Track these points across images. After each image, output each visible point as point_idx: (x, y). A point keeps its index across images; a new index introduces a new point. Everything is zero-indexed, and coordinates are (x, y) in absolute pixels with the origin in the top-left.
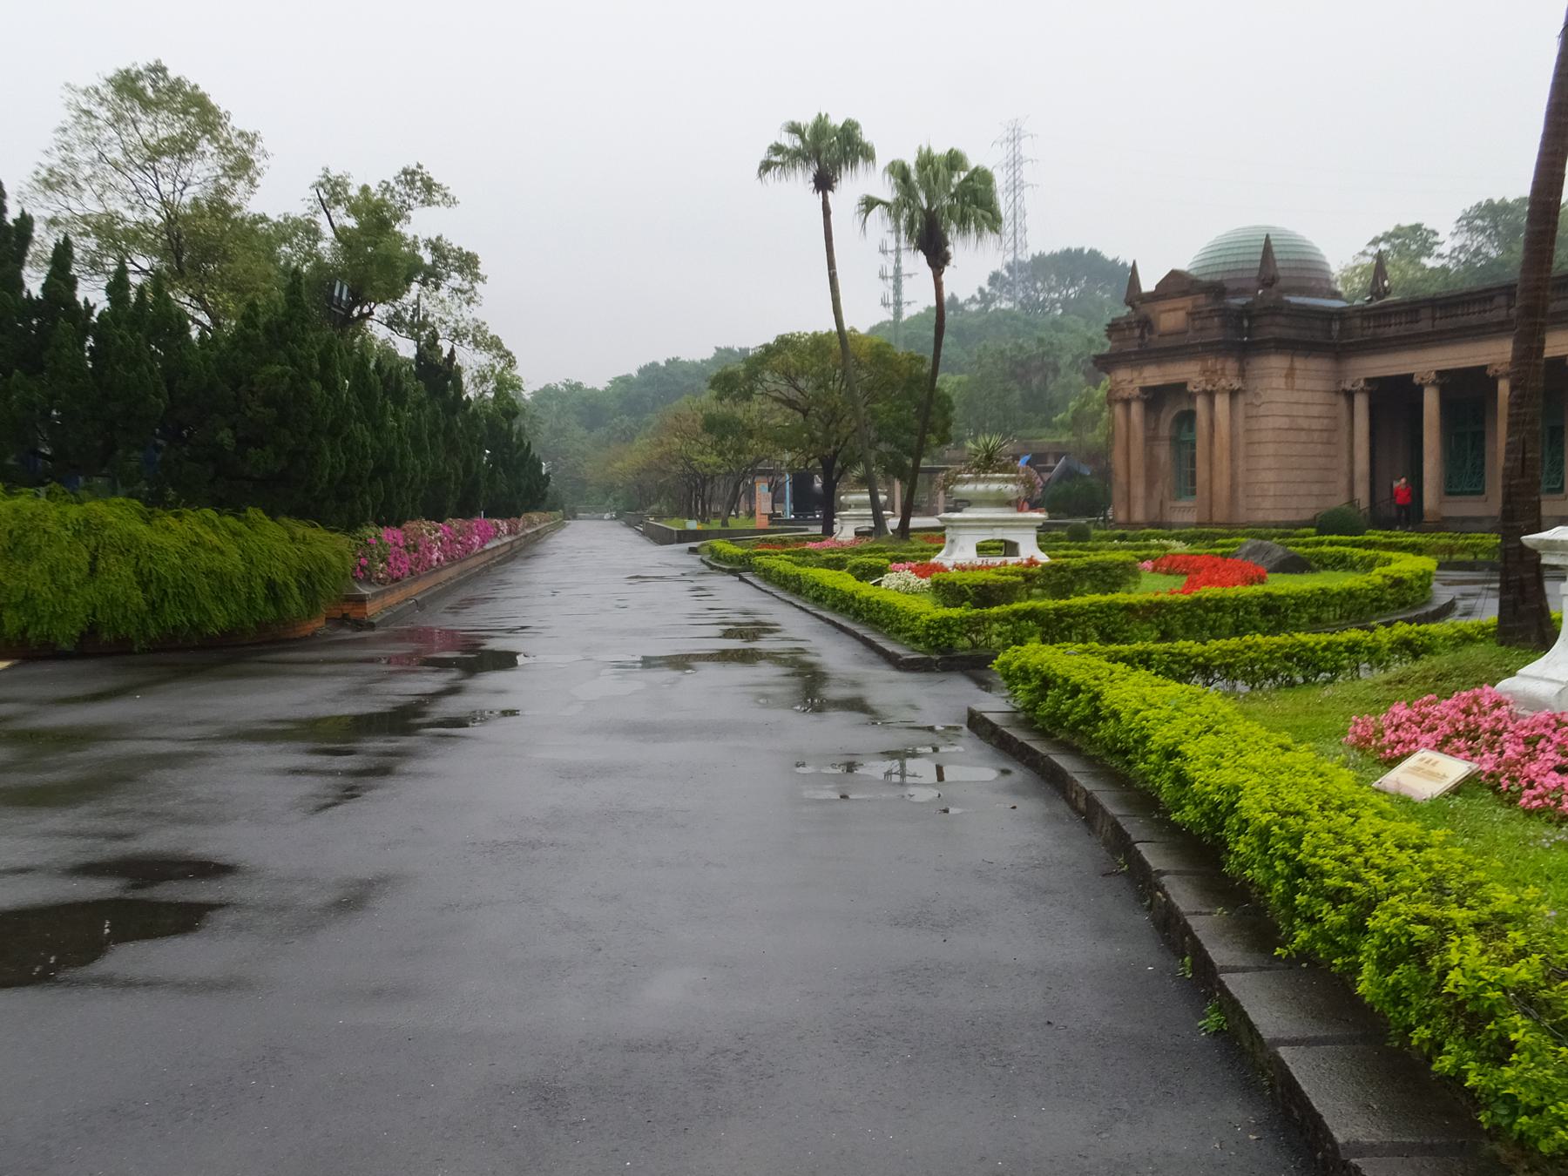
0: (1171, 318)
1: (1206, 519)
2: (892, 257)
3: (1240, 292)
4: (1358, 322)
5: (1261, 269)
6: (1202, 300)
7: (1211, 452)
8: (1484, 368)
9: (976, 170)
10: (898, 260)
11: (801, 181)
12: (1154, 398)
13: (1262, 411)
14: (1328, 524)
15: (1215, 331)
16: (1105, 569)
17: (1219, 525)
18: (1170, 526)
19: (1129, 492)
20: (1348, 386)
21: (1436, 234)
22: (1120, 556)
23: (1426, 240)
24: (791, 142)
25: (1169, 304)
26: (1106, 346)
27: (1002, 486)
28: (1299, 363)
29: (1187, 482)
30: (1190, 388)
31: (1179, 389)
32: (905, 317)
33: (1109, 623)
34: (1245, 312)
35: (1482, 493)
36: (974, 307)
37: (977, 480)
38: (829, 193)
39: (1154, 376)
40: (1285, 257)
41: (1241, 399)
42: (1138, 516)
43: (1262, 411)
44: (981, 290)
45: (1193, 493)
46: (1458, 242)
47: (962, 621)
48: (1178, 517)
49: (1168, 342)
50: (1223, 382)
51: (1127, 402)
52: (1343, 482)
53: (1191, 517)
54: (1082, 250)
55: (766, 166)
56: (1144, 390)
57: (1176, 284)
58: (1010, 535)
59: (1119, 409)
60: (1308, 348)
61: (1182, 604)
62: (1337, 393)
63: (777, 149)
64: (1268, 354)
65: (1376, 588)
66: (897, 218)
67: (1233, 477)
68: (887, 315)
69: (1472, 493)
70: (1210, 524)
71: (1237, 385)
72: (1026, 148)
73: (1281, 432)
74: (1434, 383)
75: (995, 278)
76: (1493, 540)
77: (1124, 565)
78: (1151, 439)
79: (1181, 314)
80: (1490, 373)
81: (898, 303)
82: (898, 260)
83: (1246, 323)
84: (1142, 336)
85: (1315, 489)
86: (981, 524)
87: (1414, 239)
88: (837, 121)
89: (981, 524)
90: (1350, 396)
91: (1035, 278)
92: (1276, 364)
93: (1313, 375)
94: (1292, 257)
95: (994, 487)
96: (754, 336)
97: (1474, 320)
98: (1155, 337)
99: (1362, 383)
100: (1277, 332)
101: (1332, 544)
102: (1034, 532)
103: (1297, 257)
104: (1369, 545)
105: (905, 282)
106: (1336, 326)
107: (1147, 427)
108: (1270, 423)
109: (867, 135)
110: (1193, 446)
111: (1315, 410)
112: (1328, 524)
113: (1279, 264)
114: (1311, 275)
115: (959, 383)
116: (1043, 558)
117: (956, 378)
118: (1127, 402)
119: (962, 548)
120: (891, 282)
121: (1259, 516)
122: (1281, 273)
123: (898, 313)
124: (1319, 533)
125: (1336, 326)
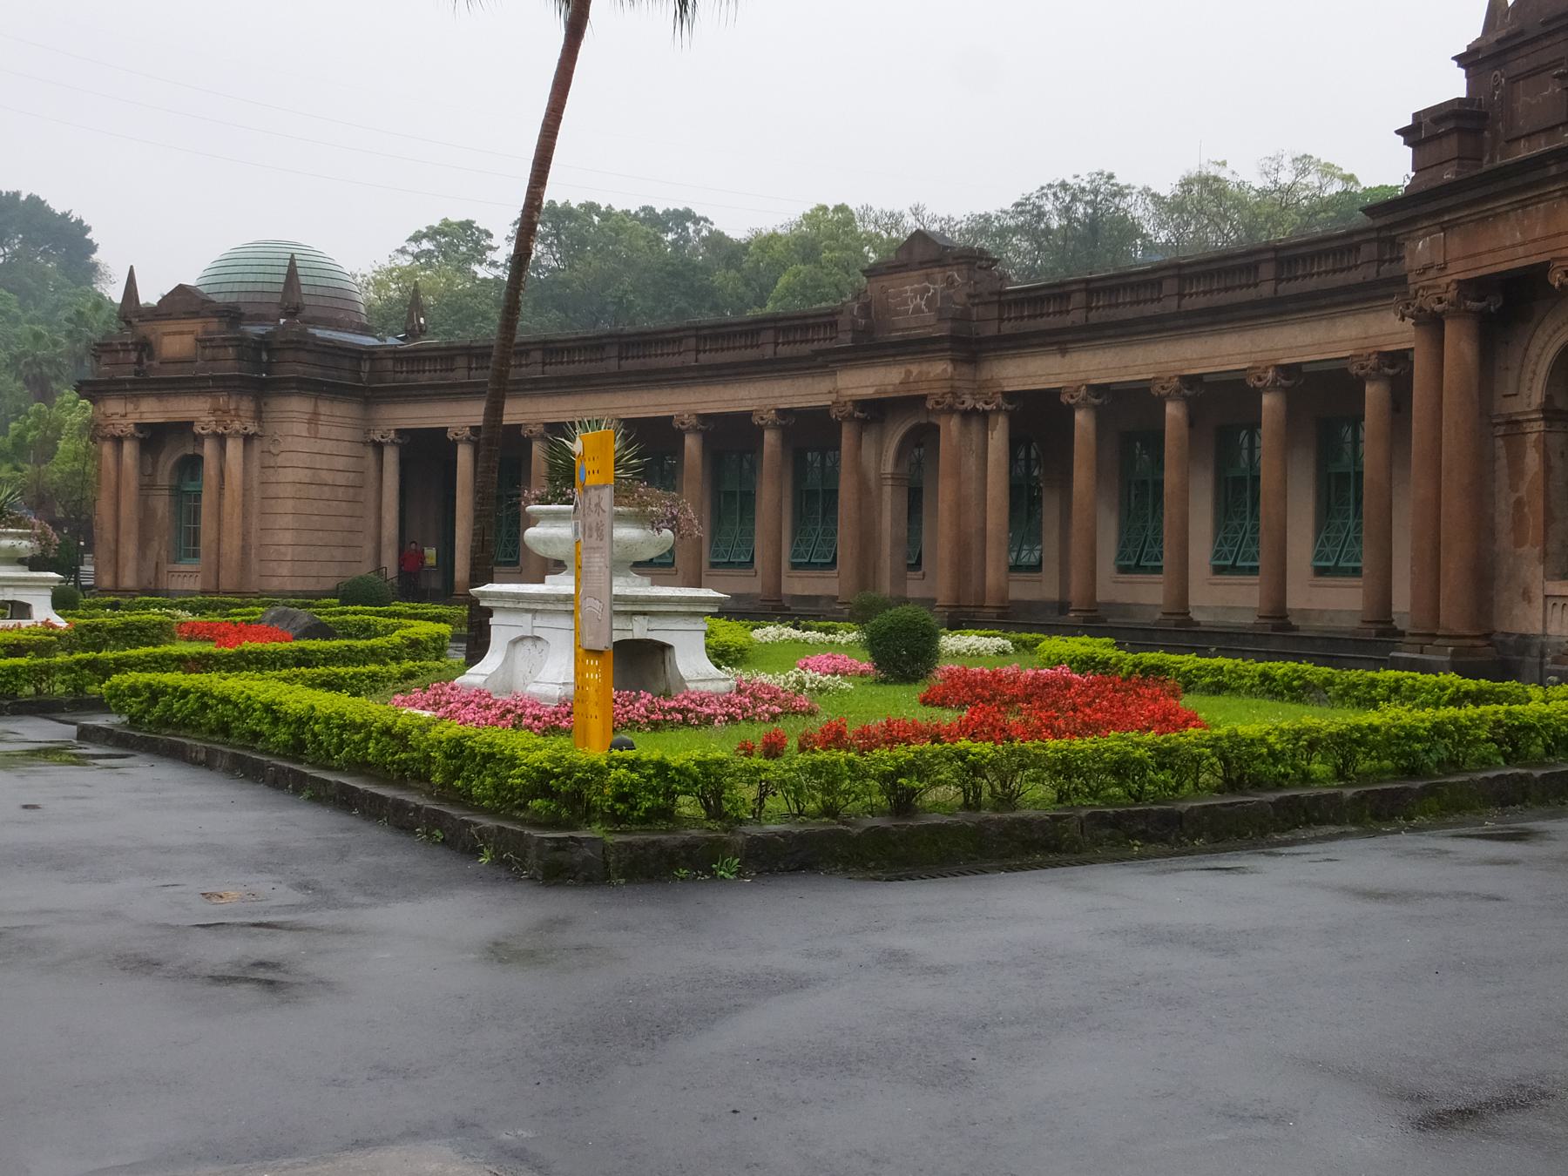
0: (176, 343)
1: (211, 587)
3: (259, 319)
4: (390, 364)
6: (214, 324)
7: (220, 505)
12: (152, 437)
13: (280, 460)
14: (351, 594)
15: (228, 364)
16: (141, 629)
17: (226, 593)
18: (168, 594)
19: (117, 552)
20: (377, 438)
21: (490, 236)
23: (477, 243)
25: (172, 326)
27: (16, 542)
28: (325, 408)
29: (188, 543)
30: (197, 429)
31: (183, 428)
34: (264, 343)
35: (516, 563)
39: (153, 411)
40: (310, 281)
41: (256, 442)
42: (128, 581)
43: (280, 460)
45: (196, 554)
47: (29, 669)
48: (177, 584)
49: (171, 373)
50: (237, 425)
51: (118, 441)
52: (369, 548)
53: (194, 584)
54: (17, 194)
57: (182, 301)
58: (22, 596)
59: (107, 449)
61: (228, 656)
62: (365, 443)
64: (290, 395)
65: (395, 647)
67: (245, 536)
71: (252, 429)
78: (147, 487)
79: (189, 340)
80: (525, 433)
83: (265, 357)
84: (139, 362)
87: (458, 240)
90: (379, 447)
92: (296, 407)
93: (338, 417)
98: (155, 363)
99: (392, 435)
100: (300, 370)
101: (355, 613)
104: (399, 615)
106: (366, 366)
107: (142, 473)
108: (289, 475)
110: (198, 496)
111: (340, 463)
112: (351, 594)
113: (304, 290)
114: (336, 305)
116: (61, 623)
118: (118, 441)
121: (275, 584)
122: (306, 300)
124: (342, 604)
125: (366, 366)
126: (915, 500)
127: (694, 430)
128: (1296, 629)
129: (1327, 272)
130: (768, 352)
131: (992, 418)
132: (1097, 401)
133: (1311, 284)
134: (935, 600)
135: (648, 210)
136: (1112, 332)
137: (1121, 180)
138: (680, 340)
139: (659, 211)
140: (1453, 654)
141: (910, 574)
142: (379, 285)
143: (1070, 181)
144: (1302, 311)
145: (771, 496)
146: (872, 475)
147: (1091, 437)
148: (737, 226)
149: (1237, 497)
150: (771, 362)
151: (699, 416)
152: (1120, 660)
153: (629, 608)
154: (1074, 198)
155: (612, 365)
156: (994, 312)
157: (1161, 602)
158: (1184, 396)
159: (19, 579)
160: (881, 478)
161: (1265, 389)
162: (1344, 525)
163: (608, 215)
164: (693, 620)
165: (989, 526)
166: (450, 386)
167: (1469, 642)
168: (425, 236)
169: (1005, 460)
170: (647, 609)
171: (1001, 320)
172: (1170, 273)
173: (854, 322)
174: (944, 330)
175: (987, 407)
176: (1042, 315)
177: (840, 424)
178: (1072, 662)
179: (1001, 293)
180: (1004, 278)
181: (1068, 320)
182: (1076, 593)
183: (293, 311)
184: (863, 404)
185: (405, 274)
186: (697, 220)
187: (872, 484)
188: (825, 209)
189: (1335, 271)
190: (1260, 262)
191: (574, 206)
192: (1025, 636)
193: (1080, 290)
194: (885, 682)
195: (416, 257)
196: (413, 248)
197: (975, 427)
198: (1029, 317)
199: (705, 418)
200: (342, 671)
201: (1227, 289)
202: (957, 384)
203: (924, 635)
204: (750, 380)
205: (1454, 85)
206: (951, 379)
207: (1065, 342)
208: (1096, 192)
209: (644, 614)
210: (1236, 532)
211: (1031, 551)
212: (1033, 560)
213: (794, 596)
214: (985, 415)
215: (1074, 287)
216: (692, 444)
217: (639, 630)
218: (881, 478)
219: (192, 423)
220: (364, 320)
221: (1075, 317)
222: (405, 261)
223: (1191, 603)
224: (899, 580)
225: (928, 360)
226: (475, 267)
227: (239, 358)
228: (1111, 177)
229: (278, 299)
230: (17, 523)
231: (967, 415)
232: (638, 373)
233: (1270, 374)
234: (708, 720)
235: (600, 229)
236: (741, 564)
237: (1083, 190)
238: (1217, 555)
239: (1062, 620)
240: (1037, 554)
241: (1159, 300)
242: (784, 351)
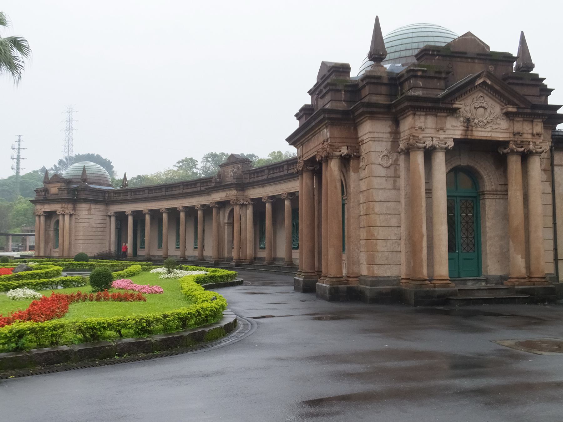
2: (17, 151)
5: (82, 176)
6: (63, 184)
8: (142, 211)
10: (19, 153)
12: (49, 215)
13: (80, 221)
18: (53, 257)
21: (197, 161)
23: (194, 163)
28: (93, 206)
30: (58, 213)
34: (76, 189)
35: (144, 248)
39: (48, 208)
40: (91, 175)
41: (73, 216)
42: (42, 254)
43: (80, 221)
44: (55, 166)
46: (203, 164)
49: (53, 197)
50: (67, 212)
51: (39, 216)
52: (107, 244)
54: (93, 155)
56: (45, 212)
59: (37, 218)
60: (96, 202)
68: (13, 173)
70: (63, 257)
71: (72, 212)
73: (88, 229)
75: (61, 162)
76: (234, 255)
78: (47, 229)
79: (56, 189)
80: (144, 212)
81: (18, 169)
82: (19, 153)
84: (45, 195)
85: (98, 246)
87: (190, 163)
90: (110, 217)
93: (98, 210)
94: (95, 173)
97: (140, 196)
103: (100, 173)
105: (21, 160)
108: (81, 225)
111: (98, 221)
118: (39, 216)
120: (16, 161)
122: (88, 177)
123: (18, 173)
125: (107, 195)
127: (183, 211)
140: (304, 278)
142: (166, 174)
150: (199, 191)
155: (163, 193)
156: (248, 176)
160: (224, 224)
167: (310, 274)
171: (250, 178)
173: (215, 180)
174: (235, 181)
179: (249, 171)
183: (85, 181)
186: (255, 157)
188: (275, 152)
195: (179, 167)
196: (178, 165)
199: (168, 209)
205: (308, 100)
214: (246, 205)
219: (56, 211)
220: (111, 183)
225: (231, 190)
227: (68, 193)
229: (80, 177)
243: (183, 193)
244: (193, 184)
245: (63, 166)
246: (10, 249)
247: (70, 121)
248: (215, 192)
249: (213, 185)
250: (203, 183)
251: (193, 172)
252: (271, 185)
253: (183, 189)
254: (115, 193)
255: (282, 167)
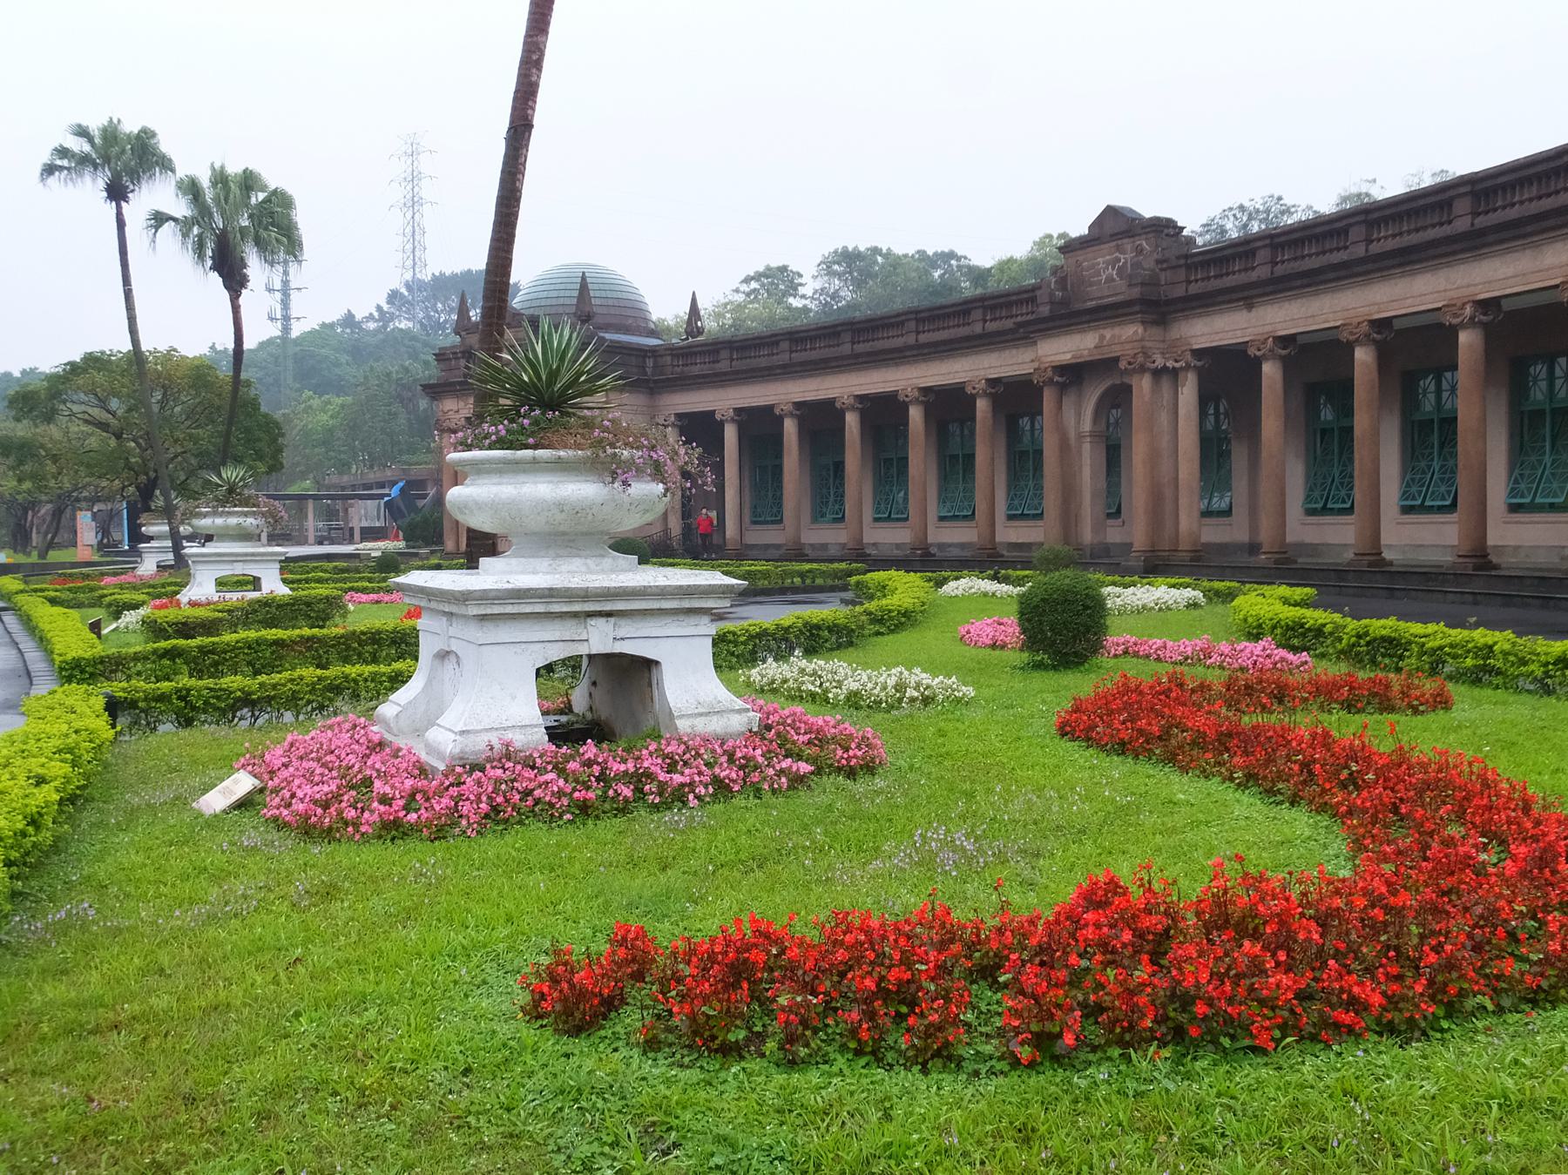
4: (669, 358)
8: (771, 407)
9: (275, 192)
10: (286, 273)
11: (92, 187)
16: (308, 604)
21: (800, 276)
22: (322, 591)
24: (79, 145)
26: (433, 373)
27: (241, 520)
32: (295, 334)
33: (259, 658)
35: (781, 521)
36: (372, 326)
37: (215, 514)
38: (124, 204)
40: (604, 302)
44: (379, 308)
46: (818, 285)
55: (49, 170)
58: (253, 570)
63: (63, 152)
66: (185, 235)
68: (274, 331)
69: (773, 522)
72: (425, 164)
74: (733, 420)
75: (393, 296)
77: (327, 600)
80: (777, 411)
81: (286, 318)
86: (220, 558)
87: (779, 280)
88: (130, 126)
89: (220, 558)
91: (436, 298)
95: (233, 521)
96: (50, 357)
102: (278, 566)
103: (615, 295)
105: (294, 295)
106: (650, 363)
109: (165, 146)
114: (630, 314)
115: (343, 406)
116: (283, 591)
117: (339, 401)
119: (200, 584)
120: (278, 296)
123: (286, 329)
125: (650, 363)
126: (1114, 457)
127: (916, 401)
128: (1496, 567)
129: (1531, 200)
130: (978, 328)
131: (1181, 375)
132: (1284, 352)
133: (1513, 213)
134: (1131, 545)
135: (922, 253)
136: (1299, 283)
137: (1288, 201)
138: (902, 323)
139: (930, 253)
141: (1110, 522)
143: (1247, 204)
144: (1502, 241)
145: (988, 455)
146: (1072, 434)
147: (1279, 386)
148: (984, 258)
149: (1431, 438)
150: (980, 337)
151: (921, 389)
152: (1337, 627)
153: (577, 608)
154: (1250, 218)
155: (846, 349)
156: (1181, 274)
157: (1352, 541)
158: (1374, 340)
159: (246, 555)
160: (1080, 437)
161: (1462, 326)
162: (1540, 462)
163: (888, 254)
164: (693, 620)
165: (1181, 476)
166: (716, 375)
168: (753, 278)
169: (1195, 414)
170: (608, 607)
172: (1358, 219)
173: (1051, 295)
174: (1135, 293)
175: (1177, 365)
176: (1228, 274)
177: (1041, 389)
178: (1274, 627)
179: (1186, 257)
180: (1190, 241)
181: (1254, 276)
182: (1265, 536)
184: (1062, 369)
185: (739, 307)
186: (959, 259)
187: (1073, 442)
188: (1050, 237)
189: (1540, 198)
190: (1351, 225)
191: (862, 249)
192: (1217, 585)
193: (1465, 194)
194: (1039, 666)
195: (748, 295)
196: (744, 288)
197: (1166, 384)
198: (1216, 277)
199: (926, 391)
200: (352, 670)
201: (1417, 230)
202: (1148, 344)
203: (1086, 607)
204: (962, 355)
206: (1142, 340)
207: (1252, 297)
208: (1268, 211)
209: (609, 614)
210: (1424, 472)
211: (1221, 498)
212: (1224, 505)
213: (1010, 544)
214: (1175, 372)
215: (1259, 244)
216: (915, 414)
217: (600, 638)
218: (1080, 437)
221: (1262, 272)
222: (740, 298)
223: (1490, 542)
224: (1098, 528)
226: (791, 300)
228: (1280, 198)
230: (245, 502)
231: (1158, 373)
232: (869, 354)
233: (1468, 310)
234: (678, 797)
235: (883, 267)
236: (965, 517)
237: (1257, 211)
238: (1405, 495)
239: (1253, 561)
240: (1227, 500)
241: (1346, 248)
242: (992, 326)
243: (918, 346)
244: (956, 314)
245: (399, 309)
246: (311, 539)
247: (414, 179)
248: (1050, 336)
249: (1045, 310)
250: (993, 308)
251: (789, 308)
252: (1289, 299)
253: (918, 333)
254: (677, 356)
255: (1343, 232)
